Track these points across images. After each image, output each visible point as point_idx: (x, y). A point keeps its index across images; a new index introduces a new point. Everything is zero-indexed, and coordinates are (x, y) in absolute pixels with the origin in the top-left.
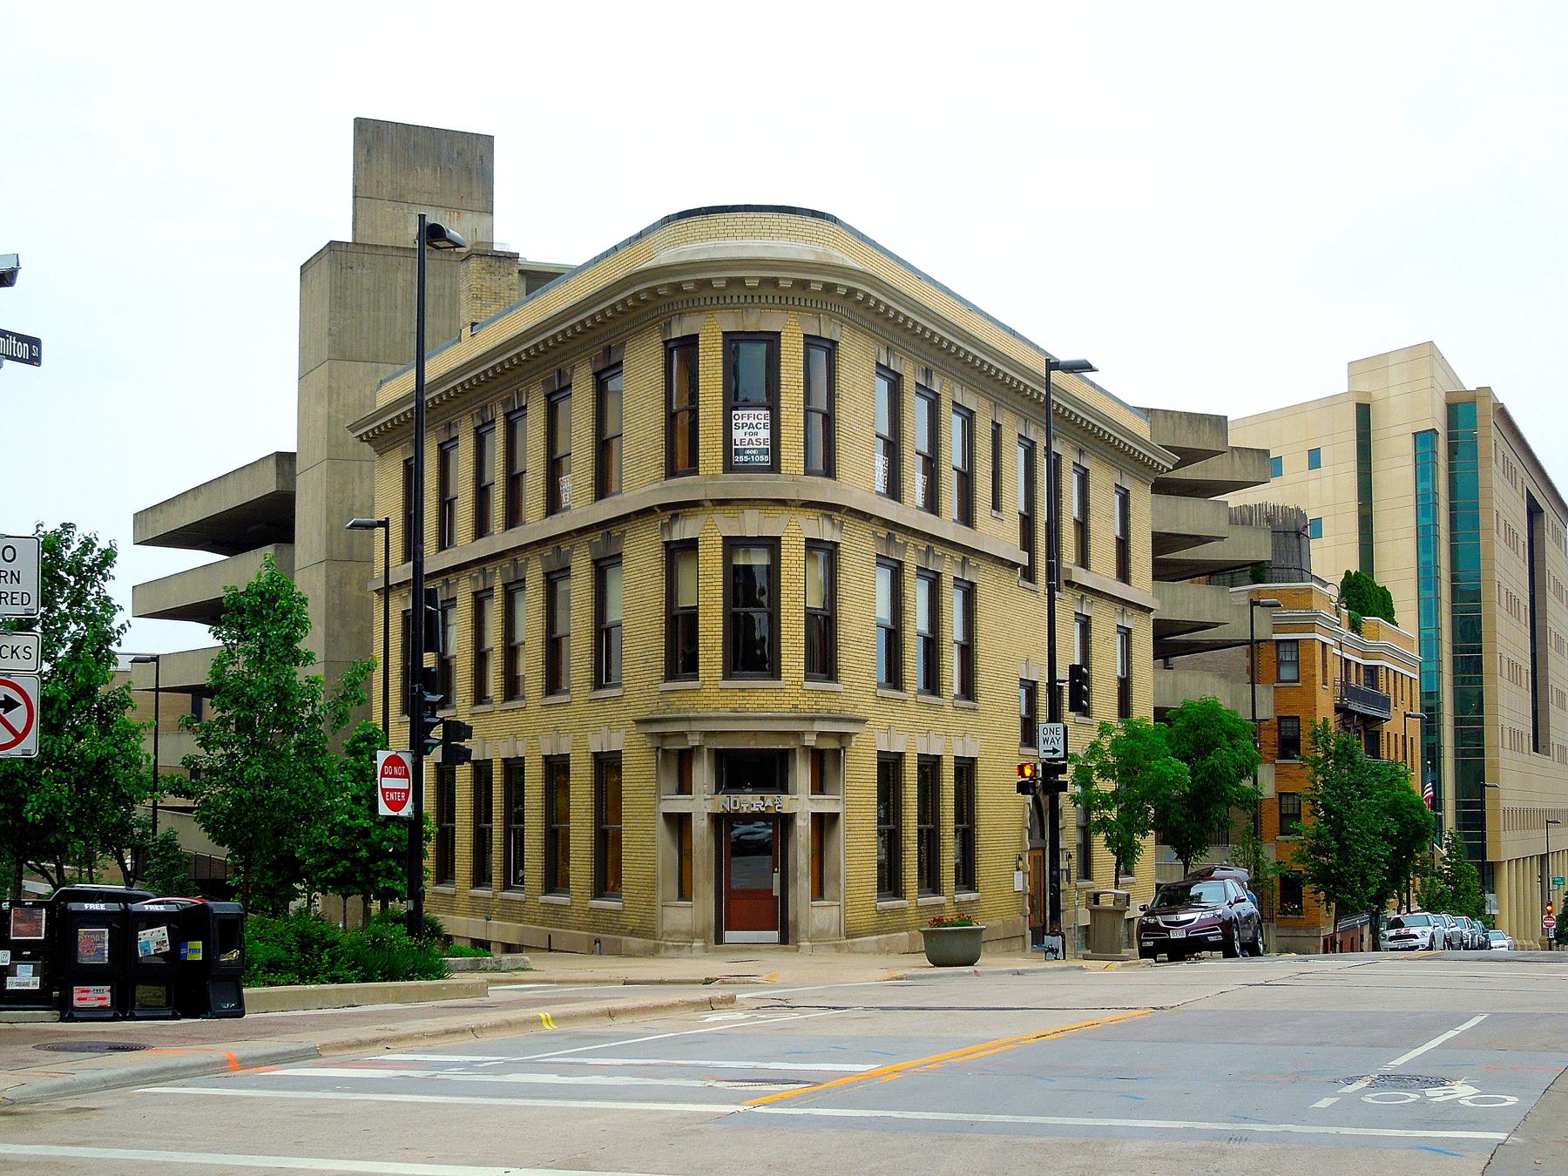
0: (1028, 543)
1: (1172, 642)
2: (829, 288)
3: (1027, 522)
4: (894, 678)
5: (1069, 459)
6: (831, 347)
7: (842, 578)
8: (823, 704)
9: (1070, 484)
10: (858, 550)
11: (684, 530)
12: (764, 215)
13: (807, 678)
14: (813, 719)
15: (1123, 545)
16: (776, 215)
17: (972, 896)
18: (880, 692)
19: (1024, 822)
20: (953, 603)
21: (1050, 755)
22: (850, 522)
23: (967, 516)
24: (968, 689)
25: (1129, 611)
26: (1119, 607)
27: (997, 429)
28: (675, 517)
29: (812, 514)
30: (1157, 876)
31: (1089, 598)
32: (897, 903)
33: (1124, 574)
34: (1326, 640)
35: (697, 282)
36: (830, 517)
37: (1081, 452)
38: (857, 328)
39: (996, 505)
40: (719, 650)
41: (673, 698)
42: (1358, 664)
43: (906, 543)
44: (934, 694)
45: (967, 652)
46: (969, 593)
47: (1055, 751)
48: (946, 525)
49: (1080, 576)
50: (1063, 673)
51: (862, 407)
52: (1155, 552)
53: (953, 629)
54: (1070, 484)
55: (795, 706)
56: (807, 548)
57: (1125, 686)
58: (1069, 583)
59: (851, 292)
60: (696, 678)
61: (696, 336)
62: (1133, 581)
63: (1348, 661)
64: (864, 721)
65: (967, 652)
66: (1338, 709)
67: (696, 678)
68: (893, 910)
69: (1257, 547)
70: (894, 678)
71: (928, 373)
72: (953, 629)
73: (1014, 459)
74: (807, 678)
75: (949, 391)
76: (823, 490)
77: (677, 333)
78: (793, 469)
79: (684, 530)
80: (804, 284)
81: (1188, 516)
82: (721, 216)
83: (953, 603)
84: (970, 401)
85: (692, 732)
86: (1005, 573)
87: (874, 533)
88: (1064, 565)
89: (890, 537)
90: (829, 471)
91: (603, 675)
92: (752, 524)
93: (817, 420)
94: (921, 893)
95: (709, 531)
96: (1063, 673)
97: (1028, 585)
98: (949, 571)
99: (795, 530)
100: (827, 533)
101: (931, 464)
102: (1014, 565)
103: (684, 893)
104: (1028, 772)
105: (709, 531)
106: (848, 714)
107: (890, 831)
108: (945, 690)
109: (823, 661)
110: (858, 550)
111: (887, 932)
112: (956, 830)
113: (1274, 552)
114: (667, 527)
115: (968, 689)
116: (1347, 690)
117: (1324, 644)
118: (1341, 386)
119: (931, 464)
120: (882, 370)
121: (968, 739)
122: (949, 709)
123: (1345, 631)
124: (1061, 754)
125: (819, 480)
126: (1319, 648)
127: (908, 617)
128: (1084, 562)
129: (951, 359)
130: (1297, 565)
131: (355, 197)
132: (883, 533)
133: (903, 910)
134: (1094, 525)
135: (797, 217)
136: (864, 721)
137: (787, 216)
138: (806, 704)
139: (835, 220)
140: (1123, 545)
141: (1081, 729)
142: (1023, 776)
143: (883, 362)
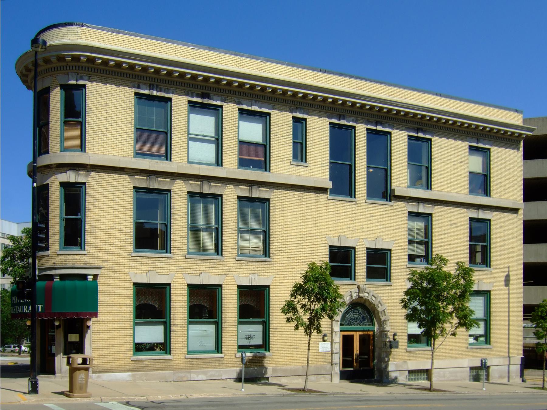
8: (70, 261)
64: (100, 268)
85: (90, 275)
92: (71, 177)
111: (146, 371)
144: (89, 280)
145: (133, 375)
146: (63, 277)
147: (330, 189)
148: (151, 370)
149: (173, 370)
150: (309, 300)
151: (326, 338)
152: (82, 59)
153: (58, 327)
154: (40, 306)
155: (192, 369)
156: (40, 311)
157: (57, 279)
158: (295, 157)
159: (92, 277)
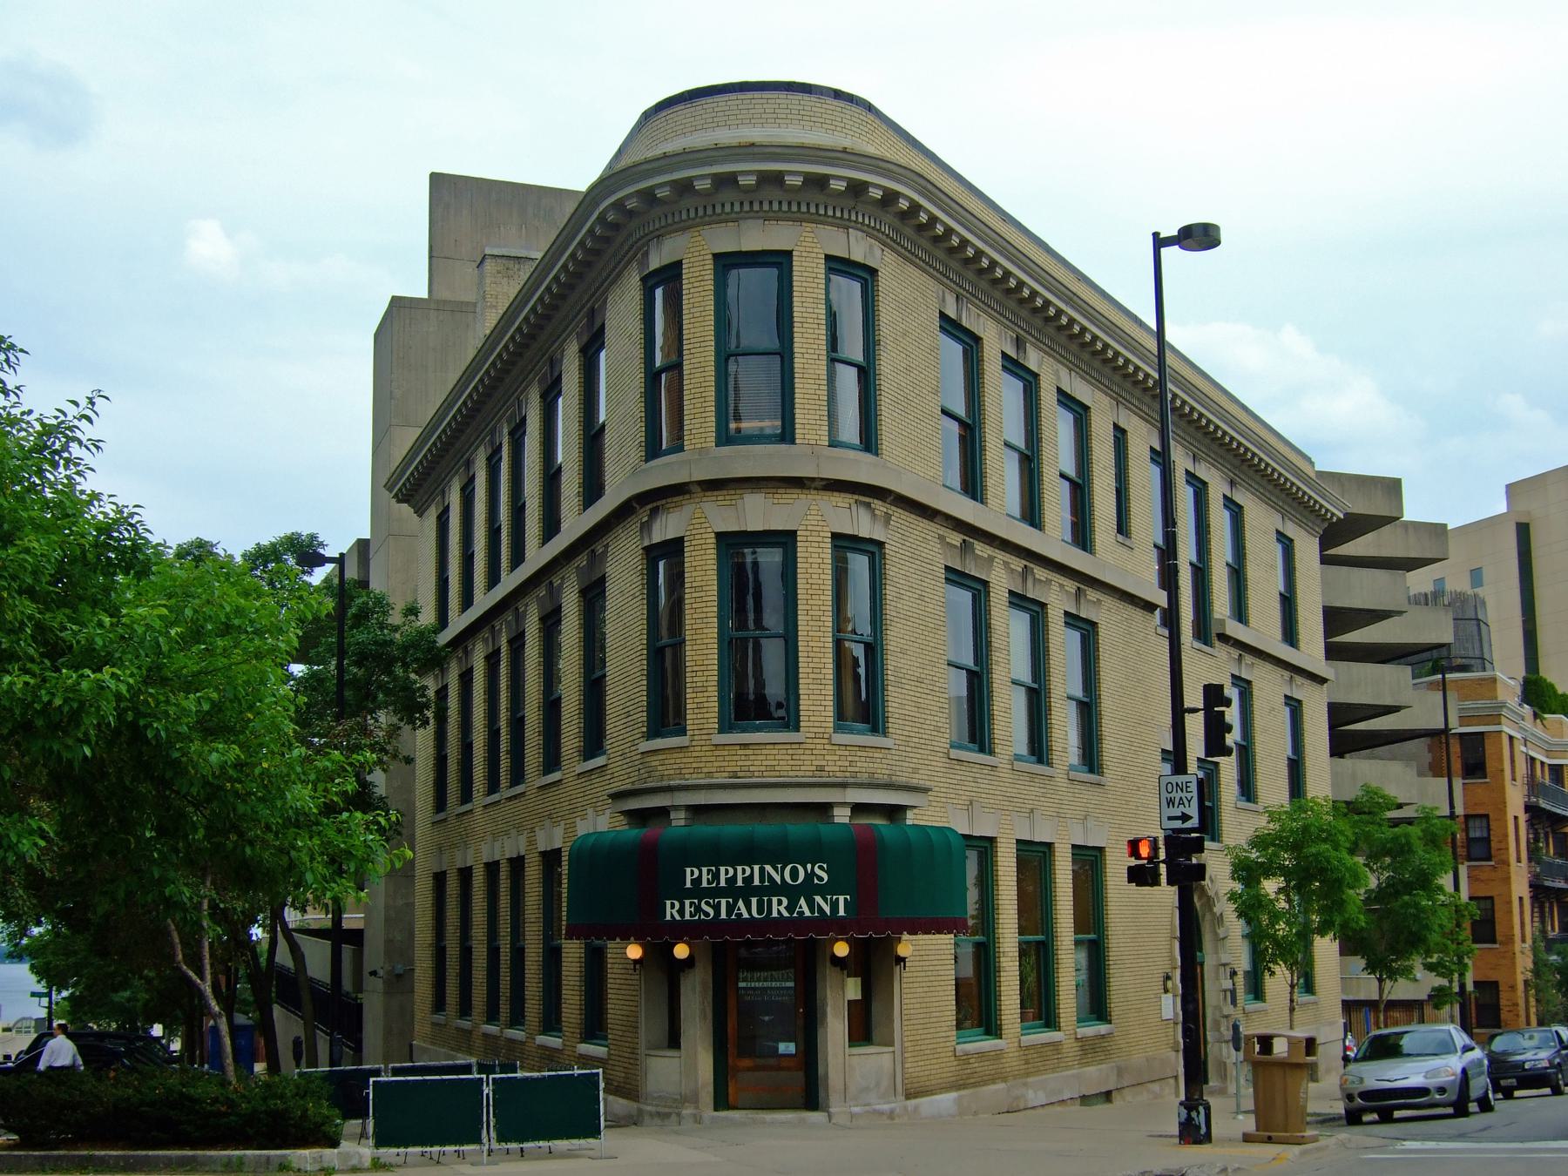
0: (1168, 578)
1: (1351, 733)
2: (857, 189)
3: (1167, 552)
4: (977, 728)
5: (1217, 489)
6: (866, 275)
7: (890, 592)
8: (864, 766)
9: (1220, 520)
10: (917, 557)
11: (666, 528)
12: (766, 94)
13: (838, 729)
14: (844, 785)
15: (1288, 602)
16: (783, 95)
17: (1103, 1028)
18: (954, 753)
19: (1172, 931)
20: (1064, 646)
21: (1178, 824)
22: (900, 516)
23: (1082, 535)
24: (1091, 756)
25: (1299, 679)
26: (1287, 674)
27: (1120, 434)
28: (654, 513)
29: (842, 500)
30: (1344, 990)
31: (1248, 659)
32: (989, 1044)
33: (1290, 634)
34: (1513, 733)
35: (673, 183)
36: (868, 505)
37: (1232, 484)
38: (909, 257)
39: (1123, 527)
40: (713, 692)
41: (654, 761)
42: (1542, 763)
43: (991, 559)
44: (1040, 761)
45: (1088, 711)
46: (1087, 631)
47: (1185, 818)
48: (1054, 539)
49: (1234, 629)
50: (1193, 697)
51: (919, 370)
52: (1329, 632)
53: (1065, 680)
54: (1220, 520)
55: (821, 769)
56: (835, 547)
57: (1296, 768)
58: (1224, 638)
59: (890, 198)
60: (683, 732)
61: (679, 264)
62: (1302, 645)
63: (1533, 759)
64: (925, 790)
65: (1088, 711)
66: (1528, 808)
67: (683, 732)
68: (981, 1055)
69: (1437, 629)
70: (977, 728)
71: (1019, 343)
72: (1065, 680)
73: (1145, 478)
74: (838, 729)
75: (1052, 374)
76: (861, 469)
77: (655, 263)
78: (812, 438)
79: (666, 528)
80: (820, 182)
81: (1362, 590)
82: (709, 99)
83: (1064, 646)
84: (1082, 391)
85: (676, 808)
86: (1138, 614)
87: (941, 538)
88: (1216, 616)
89: (965, 548)
90: (869, 440)
91: (594, 742)
92: (757, 513)
93: (848, 378)
94: (1025, 1030)
95: (698, 526)
96: (1193, 697)
97: (1250, 805)
98: (1058, 598)
99: (817, 522)
100: (864, 526)
101: (1030, 462)
102: (1149, 607)
103: (674, 1041)
104: (1144, 851)
105: (698, 526)
106: (902, 779)
107: (1091, 942)
108: (1056, 757)
109: (863, 705)
110: (917, 557)
111: (975, 1085)
112: (1077, 943)
113: (1456, 634)
114: (646, 528)
115: (1091, 756)
116: (1533, 786)
117: (1511, 738)
118: (1501, 507)
119: (1030, 462)
120: (950, 326)
121: (1091, 823)
122: (1061, 780)
123: (1528, 723)
124: (1194, 822)
125: (852, 454)
126: (1506, 741)
127: (997, 656)
128: (1240, 614)
129: (1051, 330)
130: (1477, 653)
131: (431, 257)
132: (956, 539)
133: (998, 1055)
134: (1252, 572)
135: (813, 98)
136: (925, 790)
137: (800, 96)
138: (835, 765)
139: (870, 108)
140: (1288, 602)
141: (1244, 816)
142: (1138, 857)
143: (952, 314)
144: (837, 820)
145: (959, 1101)
146: (697, 811)
147: (1164, 610)
148: (985, 1083)
149: (1004, 1079)
150: (30, 869)
151: (1169, 984)
152: (790, 180)
153: (689, 963)
154: (841, 898)
155: (1028, 1075)
156: (842, 913)
157: (679, 819)
158: (1527, 525)
159: (848, 812)
